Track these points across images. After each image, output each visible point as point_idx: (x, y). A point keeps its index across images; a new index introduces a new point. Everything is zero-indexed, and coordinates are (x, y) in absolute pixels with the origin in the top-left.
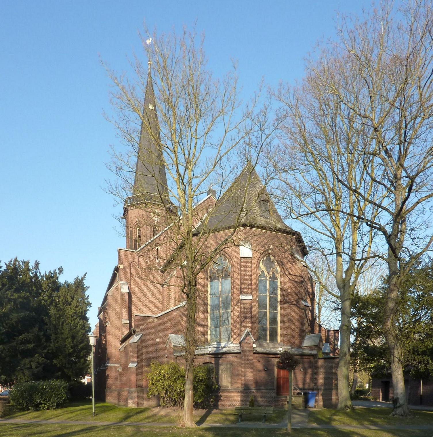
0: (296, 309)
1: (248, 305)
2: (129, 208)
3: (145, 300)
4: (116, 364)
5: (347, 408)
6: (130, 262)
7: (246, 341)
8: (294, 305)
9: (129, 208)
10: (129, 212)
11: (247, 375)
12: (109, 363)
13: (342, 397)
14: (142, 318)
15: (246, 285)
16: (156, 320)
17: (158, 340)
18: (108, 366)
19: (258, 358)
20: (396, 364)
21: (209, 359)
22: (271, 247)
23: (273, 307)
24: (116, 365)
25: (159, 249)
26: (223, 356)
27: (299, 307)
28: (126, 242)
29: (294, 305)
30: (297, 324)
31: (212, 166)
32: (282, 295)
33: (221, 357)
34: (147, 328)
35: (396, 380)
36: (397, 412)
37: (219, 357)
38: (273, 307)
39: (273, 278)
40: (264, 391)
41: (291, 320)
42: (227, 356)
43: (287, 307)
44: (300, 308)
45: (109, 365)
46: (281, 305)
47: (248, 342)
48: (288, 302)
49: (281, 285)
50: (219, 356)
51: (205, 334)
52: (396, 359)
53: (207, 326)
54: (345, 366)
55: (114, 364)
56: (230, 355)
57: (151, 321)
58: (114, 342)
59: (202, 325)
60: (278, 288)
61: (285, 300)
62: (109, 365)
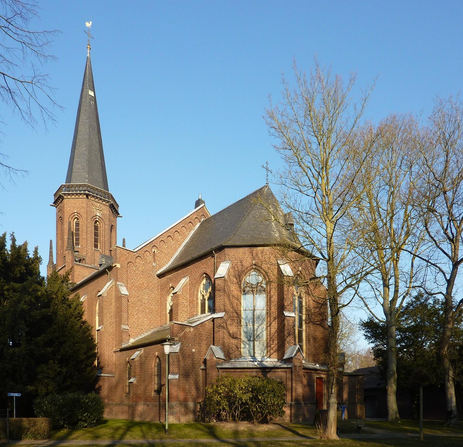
0: (321, 329)
1: (291, 321)
2: (65, 197)
3: (142, 305)
4: (109, 374)
5: (398, 420)
6: (127, 261)
7: (297, 357)
8: (318, 324)
9: (65, 197)
10: (65, 201)
11: (298, 390)
12: (101, 373)
13: (393, 410)
14: (180, 326)
15: (289, 302)
16: (192, 329)
17: (194, 350)
18: (101, 376)
19: (304, 373)
20: (451, 382)
21: (255, 373)
22: (300, 268)
23: (301, 326)
24: (110, 375)
25: (156, 252)
26: (272, 371)
27: (323, 327)
28: (57, 234)
29: (318, 324)
30: (322, 342)
31: (300, 175)
32: (308, 315)
33: (269, 372)
34: (185, 336)
35: (451, 396)
36: (452, 422)
37: (266, 372)
38: (301, 326)
39: (300, 297)
40: (309, 405)
41: (315, 339)
42: (276, 370)
43: (311, 326)
44: (324, 328)
45: (102, 375)
46: (306, 323)
47: (299, 358)
48: (312, 322)
49: (306, 305)
50: (267, 370)
51: (239, 346)
52: (450, 378)
53: (241, 339)
54: (394, 383)
55: (107, 374)
56: (279, 370)
57: (187, 330)
58: (107, 349)
59: (236, 338)
60: (303, 308)
61: (309, 321)
62: (102, 375)
